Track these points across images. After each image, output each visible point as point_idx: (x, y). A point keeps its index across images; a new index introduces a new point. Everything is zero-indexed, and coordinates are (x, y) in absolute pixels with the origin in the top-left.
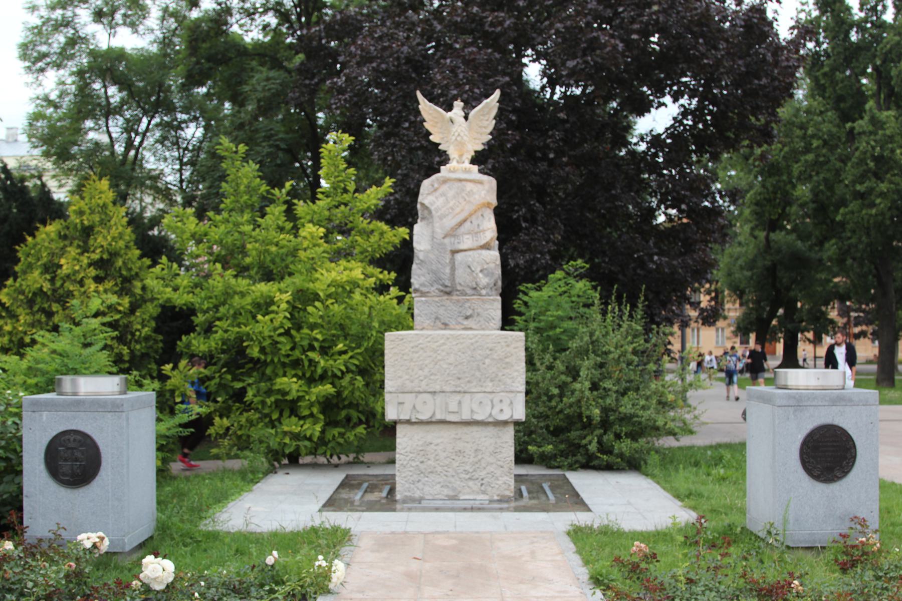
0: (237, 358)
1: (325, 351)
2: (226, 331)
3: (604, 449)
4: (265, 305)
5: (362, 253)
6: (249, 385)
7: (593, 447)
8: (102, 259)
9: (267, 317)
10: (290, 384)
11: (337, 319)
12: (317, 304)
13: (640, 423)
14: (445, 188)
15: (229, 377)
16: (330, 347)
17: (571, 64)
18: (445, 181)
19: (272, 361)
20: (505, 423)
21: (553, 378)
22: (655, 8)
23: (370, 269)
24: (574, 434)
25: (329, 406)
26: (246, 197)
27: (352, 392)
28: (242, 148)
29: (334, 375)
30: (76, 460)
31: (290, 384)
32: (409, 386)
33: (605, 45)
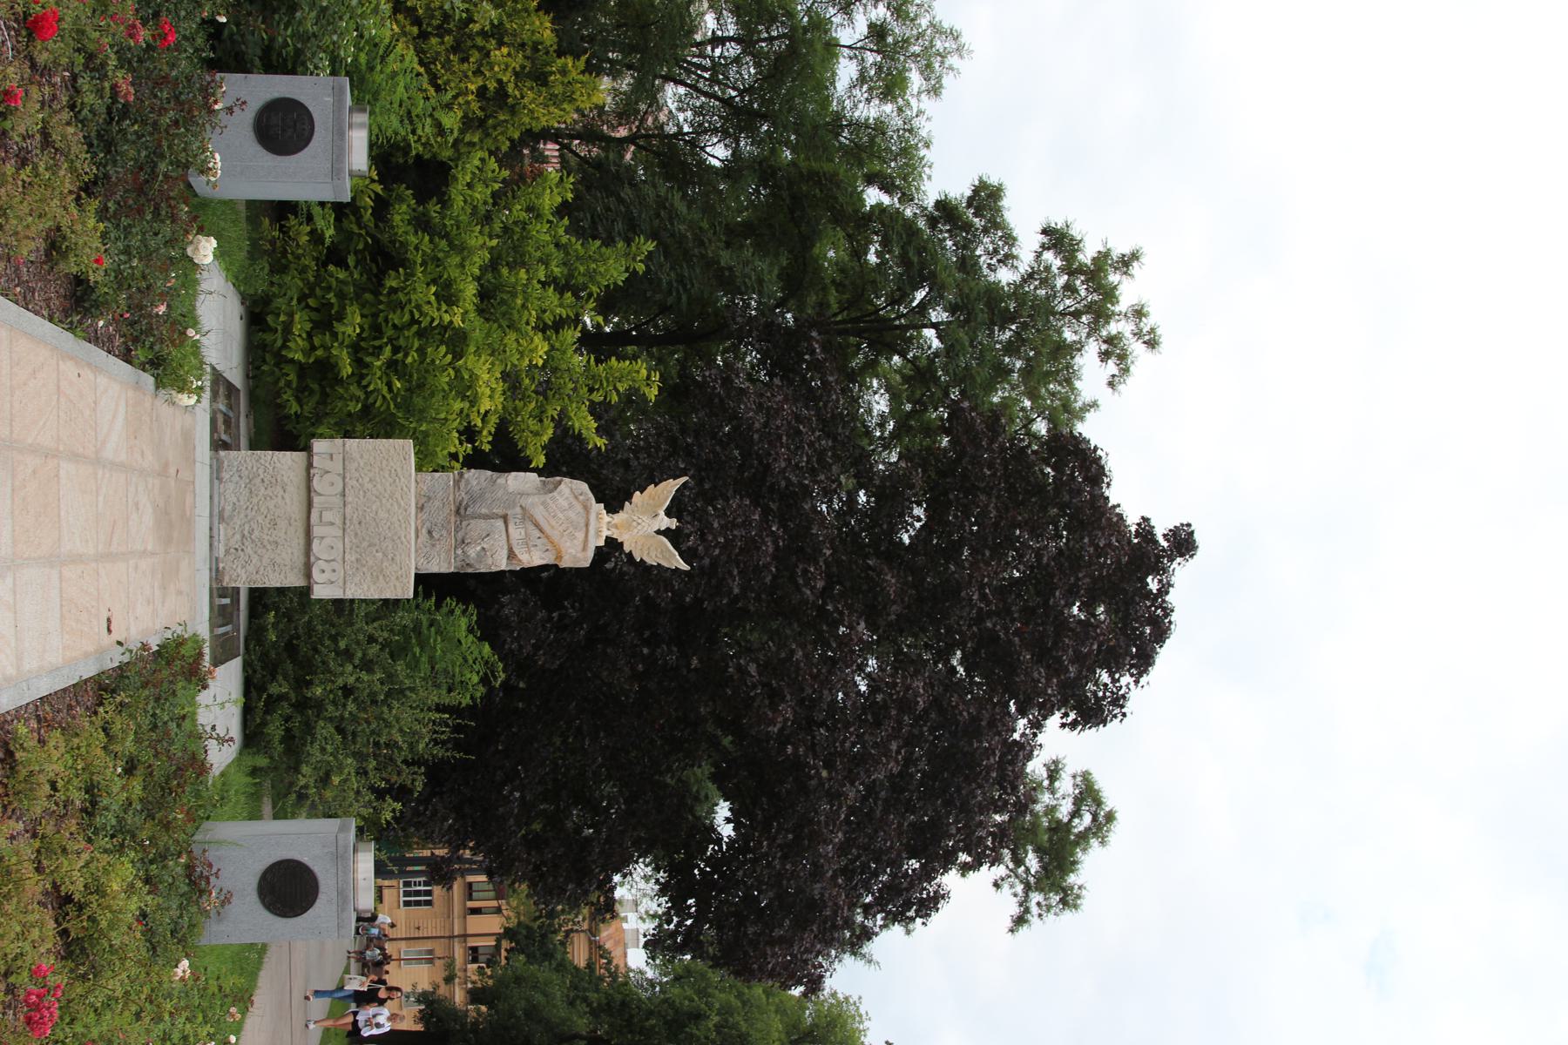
0: (386, 258)
1: (392, 365)
2: (417, 248)
3: (272, 703)
4: (448, 296)
5: (515, 409)
6: (351, 274)
7: (274, 689)
8: (507, 95)
9: (433, 298)
10: (353, 324)
11: (430, 379)
12: (450, 357)
13: (304, 745)
14: (579, 508)
15: (361, 246)
16: (396, 372)
17: (752, 668)
18: (587, 509)
19: (381, 302)
20: (308, 575)
21: (358, 643)
22: (824, 774)
23: (493, 420)
24: (289, 666)
25: (324, 370)
26: (582, 269)
27: (341, 398)
28: (641, 268)
29: (362, 377)
30: (284, 131)
31: (353, 324)
32: (352, 466)
33: (775, 710)
